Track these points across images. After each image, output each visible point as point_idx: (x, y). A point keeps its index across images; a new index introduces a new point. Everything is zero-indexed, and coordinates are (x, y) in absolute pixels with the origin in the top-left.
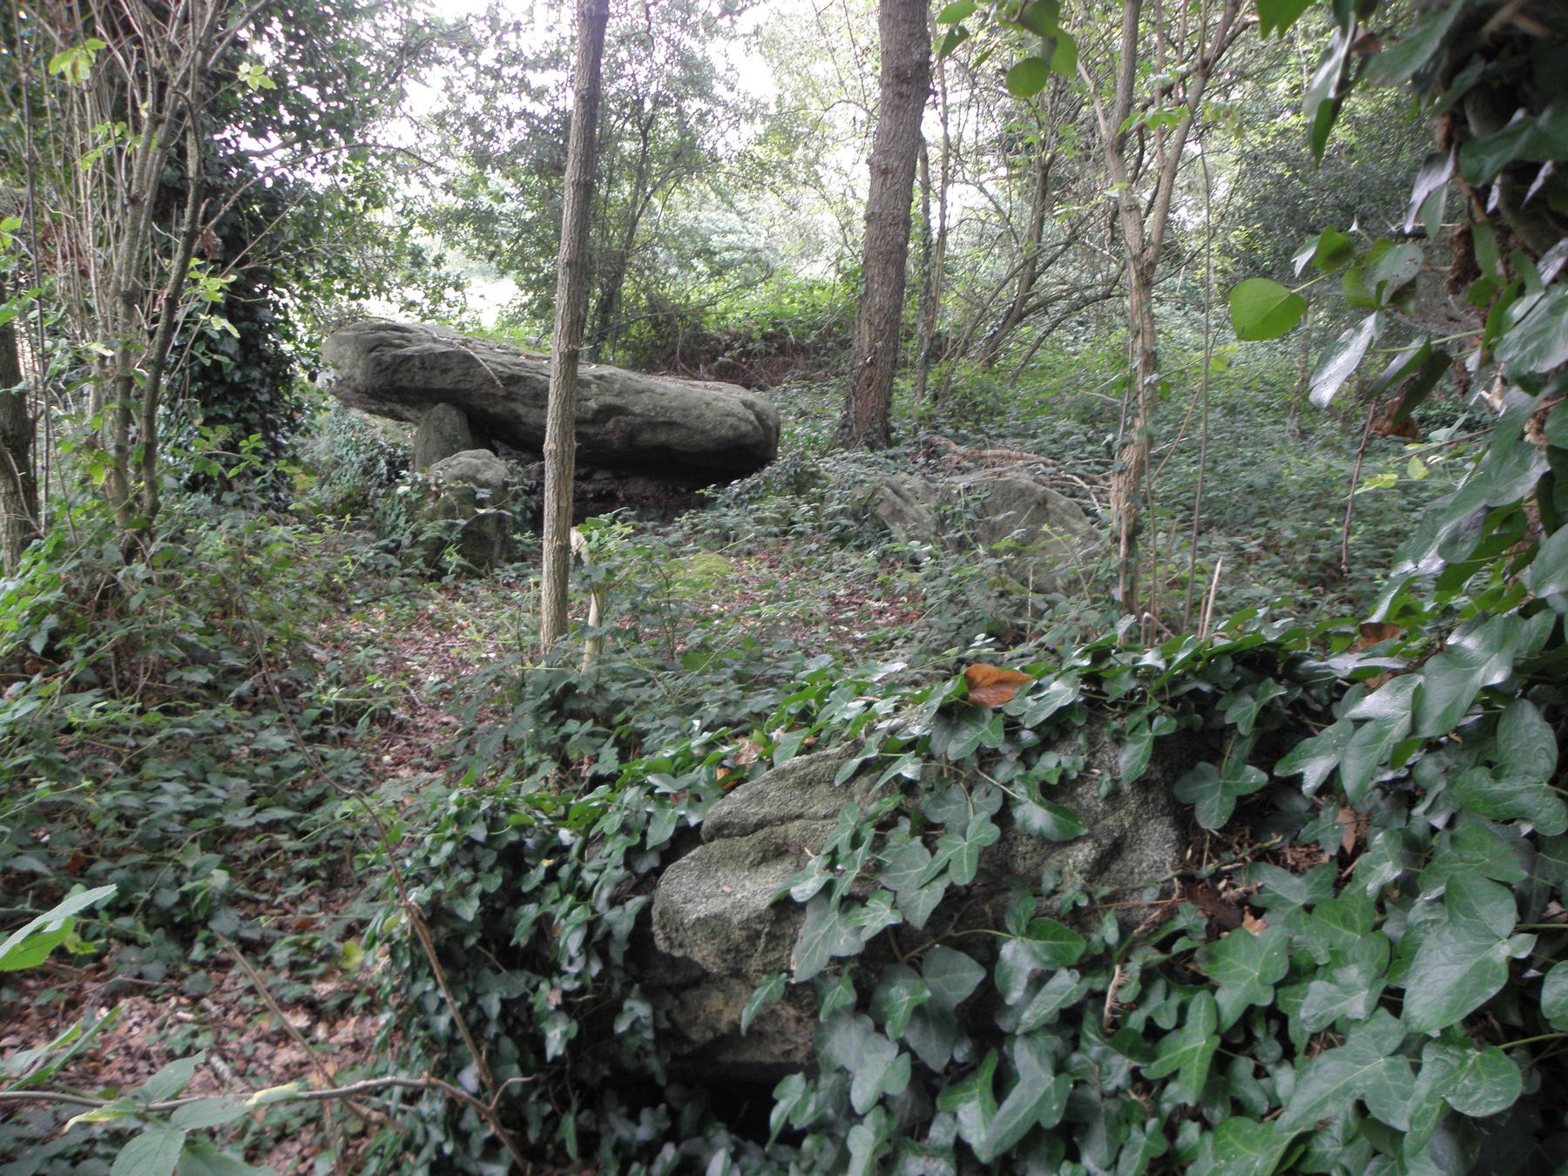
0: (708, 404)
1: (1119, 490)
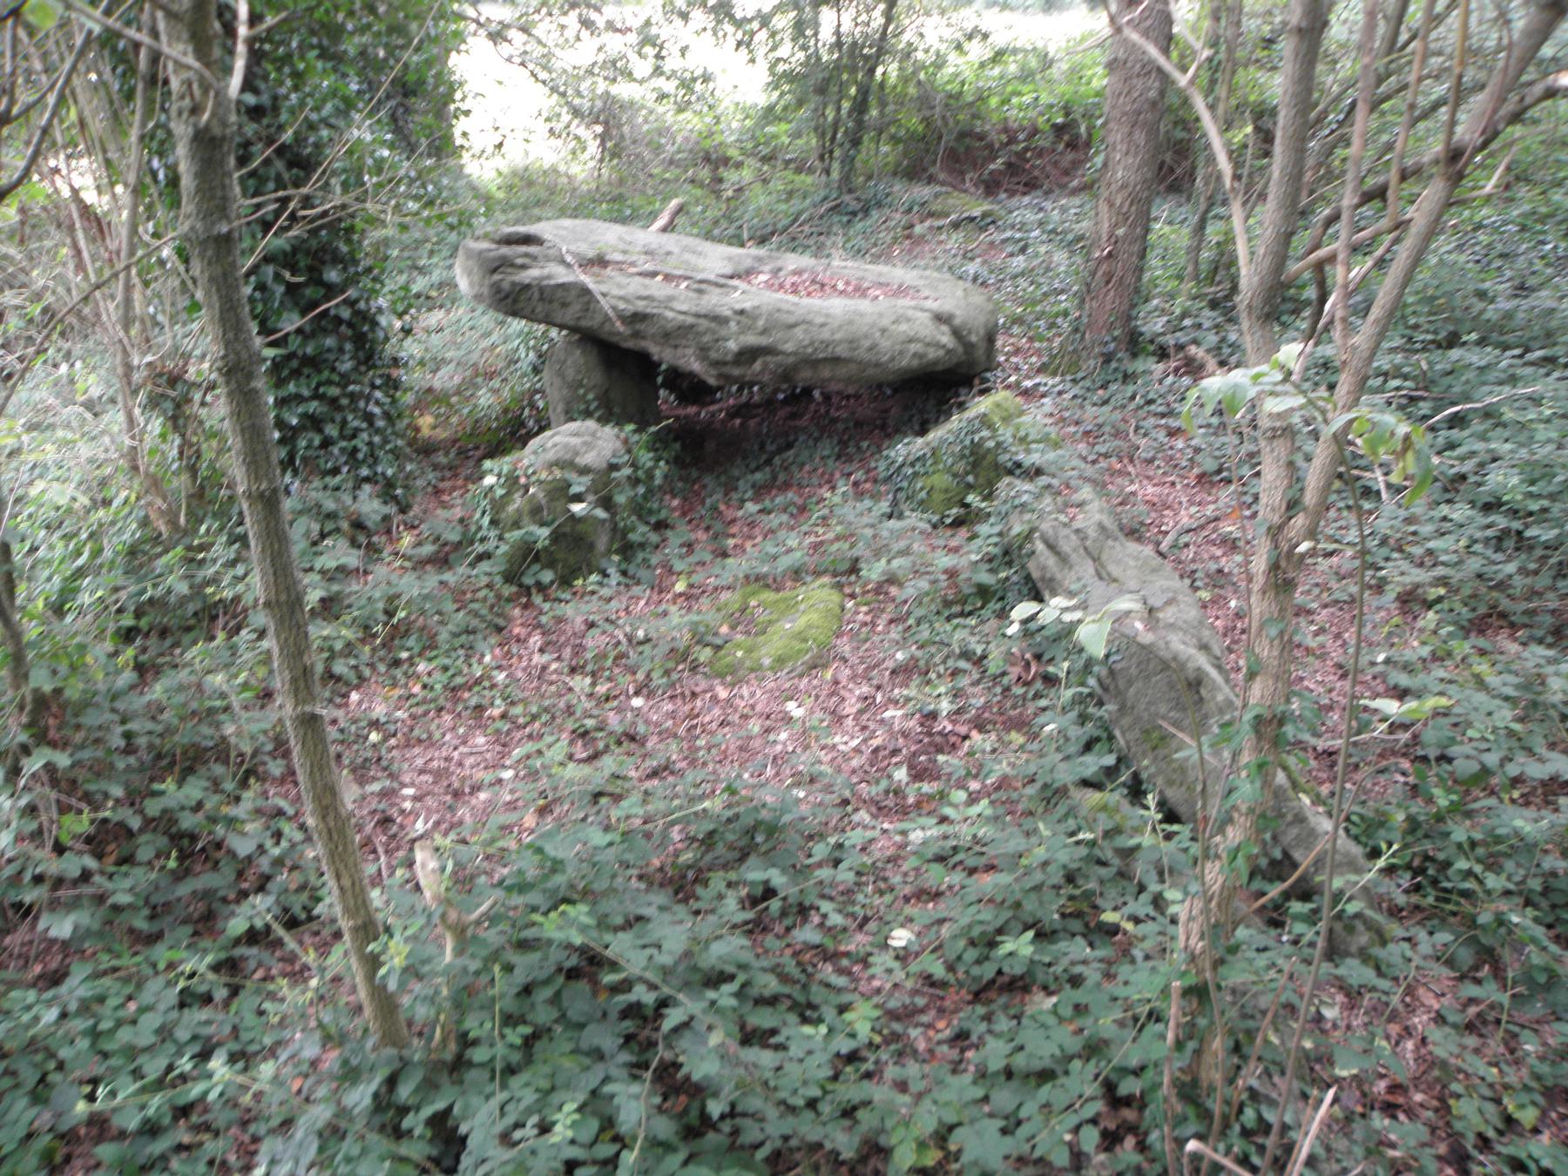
0: (884, 331)
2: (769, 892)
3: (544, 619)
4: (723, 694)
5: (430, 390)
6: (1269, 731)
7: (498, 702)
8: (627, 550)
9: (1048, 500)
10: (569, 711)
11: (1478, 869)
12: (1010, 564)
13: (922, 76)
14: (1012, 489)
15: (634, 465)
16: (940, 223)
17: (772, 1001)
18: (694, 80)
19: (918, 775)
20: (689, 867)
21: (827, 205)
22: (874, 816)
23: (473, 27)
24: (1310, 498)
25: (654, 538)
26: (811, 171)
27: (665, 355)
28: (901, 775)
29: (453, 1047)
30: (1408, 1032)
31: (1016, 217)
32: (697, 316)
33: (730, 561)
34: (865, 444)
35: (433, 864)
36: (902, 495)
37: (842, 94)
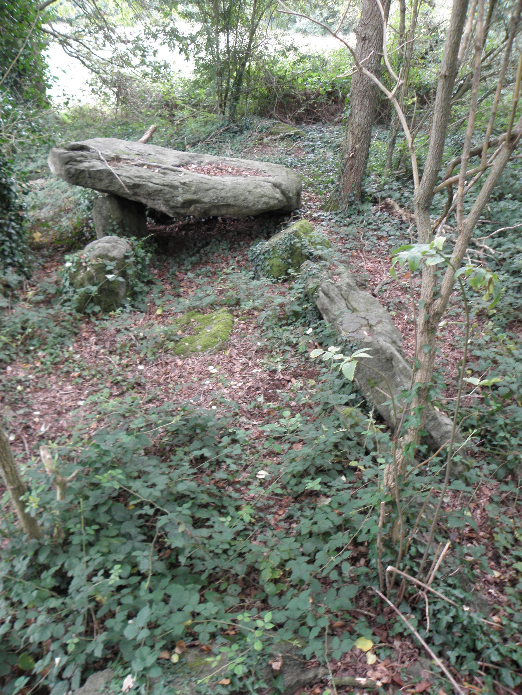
0: (250, 192)
1: (389, 473)
2: (203, 458)
3: (96, 329)
4: (180, 363)
5: (39, 220)
6: (424, 394)
7: (77, 369)
8: (134, 295)
9: (325, 272)
10: (110, 372)
11: (508, 436)
12: (308, 301)
13: (267, 67)
14: (308, 266)
15: (136, 256)
16: (276, 137)
17: (206, 506)
18: (160, 67)
19: (268, 399)
20: (167, 445)
21: (223, 128)
22: (249, 419)
23: (52, 37)
24: (444, 292)
25: (146, 289)
26: (215, 112)
27: (150, 204)
28: (261, 399)
29: (63, 535)
30: (478, 506)
31: (310, 135)
32: (164, 185)
33: (181, 299)
34: (242, 243)
35: (49, 456)
36: (259, 268)
37: (230, 76)
